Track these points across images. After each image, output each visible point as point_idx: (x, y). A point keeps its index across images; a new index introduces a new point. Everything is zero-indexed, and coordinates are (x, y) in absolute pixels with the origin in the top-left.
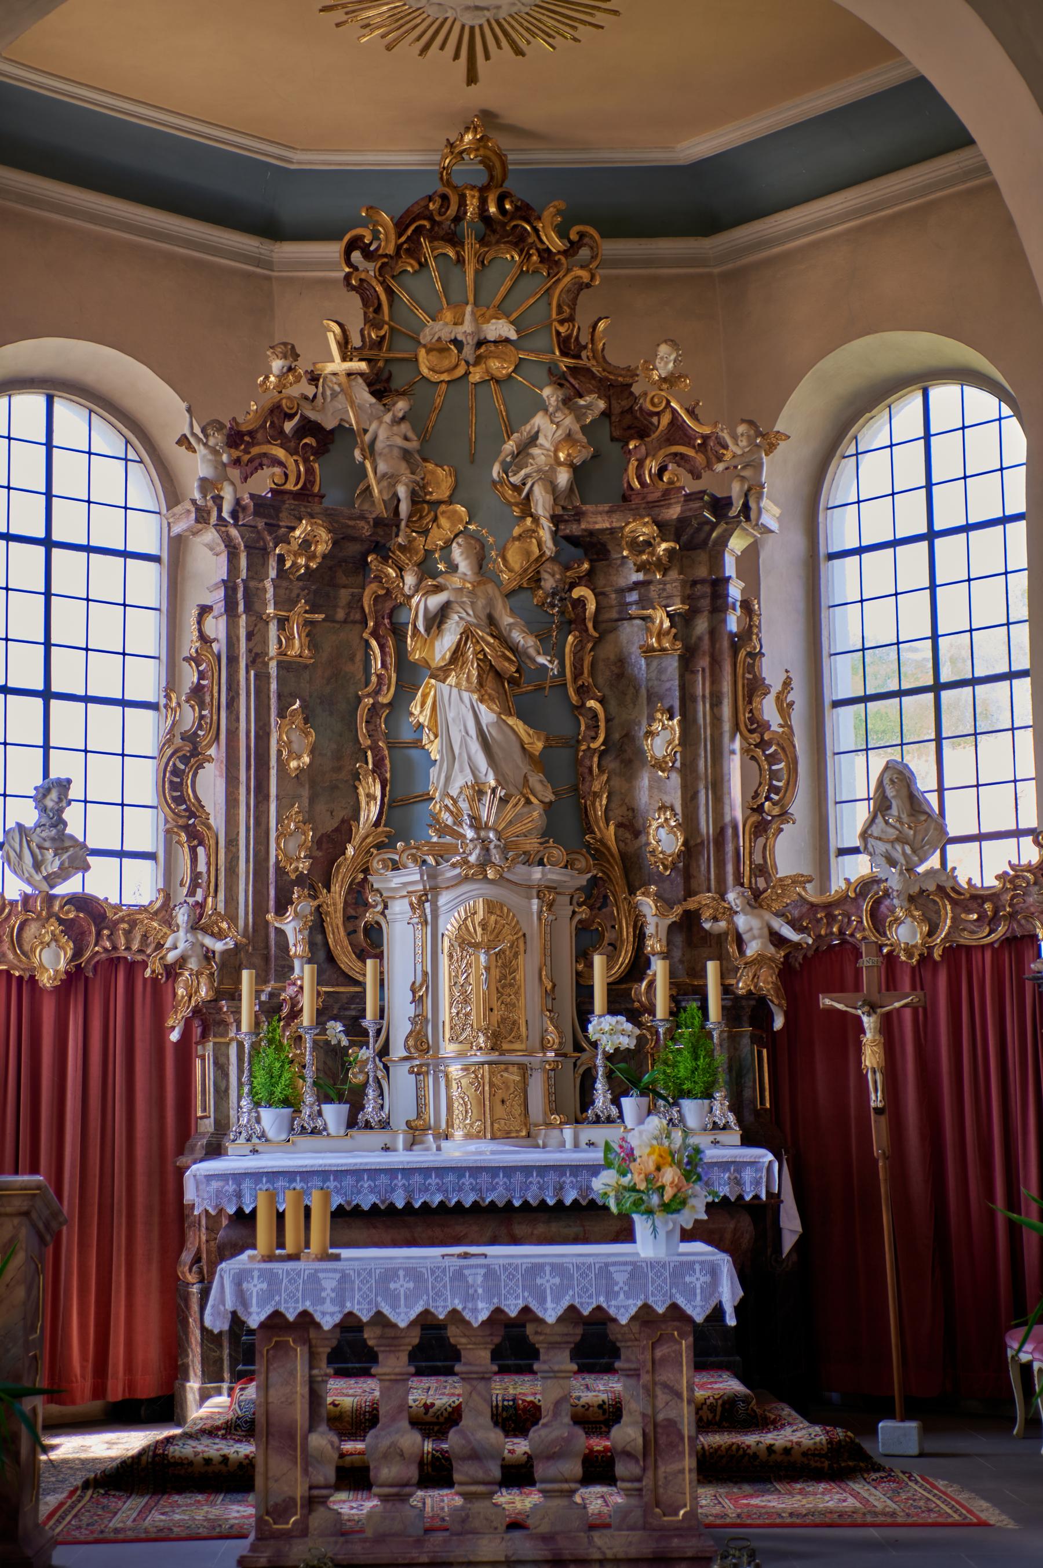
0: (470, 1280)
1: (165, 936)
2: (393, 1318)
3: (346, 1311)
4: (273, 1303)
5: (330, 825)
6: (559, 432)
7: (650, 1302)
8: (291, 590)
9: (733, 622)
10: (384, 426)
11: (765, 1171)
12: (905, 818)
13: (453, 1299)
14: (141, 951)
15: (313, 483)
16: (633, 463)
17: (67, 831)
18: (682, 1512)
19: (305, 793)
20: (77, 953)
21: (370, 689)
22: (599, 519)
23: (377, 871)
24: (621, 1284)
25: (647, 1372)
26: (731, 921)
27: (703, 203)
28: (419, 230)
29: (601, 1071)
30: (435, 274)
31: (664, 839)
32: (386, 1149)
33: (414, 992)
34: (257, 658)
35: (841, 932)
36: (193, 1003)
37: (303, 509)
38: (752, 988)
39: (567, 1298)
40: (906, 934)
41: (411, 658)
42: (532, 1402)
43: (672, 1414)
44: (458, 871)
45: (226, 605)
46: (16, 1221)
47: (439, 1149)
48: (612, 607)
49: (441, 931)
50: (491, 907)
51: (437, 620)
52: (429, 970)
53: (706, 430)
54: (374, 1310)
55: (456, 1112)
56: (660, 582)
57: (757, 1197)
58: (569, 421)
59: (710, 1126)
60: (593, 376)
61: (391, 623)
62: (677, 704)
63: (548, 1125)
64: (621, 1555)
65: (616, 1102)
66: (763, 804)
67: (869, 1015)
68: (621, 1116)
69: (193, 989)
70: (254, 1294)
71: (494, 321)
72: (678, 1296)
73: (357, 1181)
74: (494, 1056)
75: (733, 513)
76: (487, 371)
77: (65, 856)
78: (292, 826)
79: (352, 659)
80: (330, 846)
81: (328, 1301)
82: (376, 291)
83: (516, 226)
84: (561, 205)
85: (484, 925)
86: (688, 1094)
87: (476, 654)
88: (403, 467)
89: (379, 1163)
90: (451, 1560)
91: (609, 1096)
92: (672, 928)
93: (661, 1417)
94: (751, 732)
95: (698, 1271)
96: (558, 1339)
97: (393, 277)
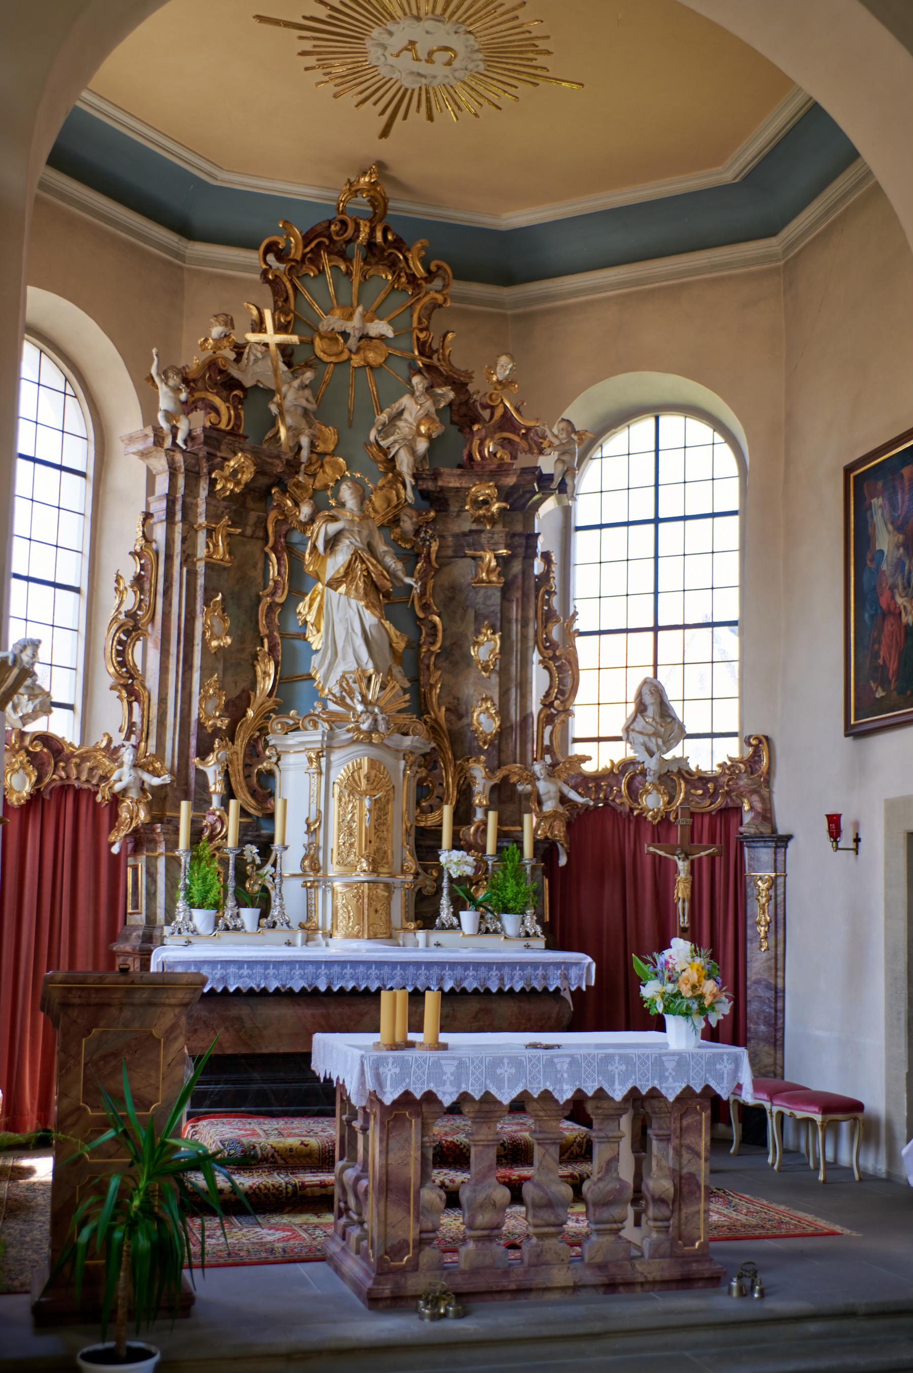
0: (558, 1066)
1: (111, 771)
2: (498, 1097)
3: (462, 1091)
4: (404, 1084)
5: (236, 692)
6: (422, 412)
7: (691, 1085)
8: (218, 508)
9: (538, 566)
10: (292, 390)
11: (585, 972)
12: (658, 719)
13: (545, 1082)
14: (87, 781)
15: (239, 427)
16: (476, 442)
17: (37, 683)
18: (697, 1244)
19: (220, 666)
20: (39, 780)
21: (268, 590)
22: (452, 480)
23: (274, 732)
24: (670, 1071)
25: (677, 1137)
26: (534, 786)
27: (506, 261)
28: (319, 245)
29: (445, 892)
30: (330, 280)
31: (484, 721)
32: (289, 944)
33: (309, 826)
34: (188, 558)
35: (606, 798)
36: (134, 825)
37: (237, 445)
38: (549, 834)
39: (631, 1081)
40: (652, 802)
41: (306, 570)
42: (451, 1142)
43: (693, 1169)
44: (350, 735)
45: (167, 514)
46: (177, 1010)
47: (327, 945)
48: (448, 547)
49: (332, 780)
50: (373, 763)
51: (332, 543)
52: (322, 809)
53: (530, 424)
54: (484, 1091)
55: (340, 918)
56: (489, 532)
57: (579, 989)
58: (429, 404)
59: (523, 934)
60: (441, 374)
61: (286, 542)
62: (498, 624)
63: (405, 929)
64: (658, 1278)
65: (456, 914)
66: (553, 702)
67: (684, 860)
68: (460, 925)
69: (135, 813)
70: (389, 1077)
71: (376, 321)
72: (710, 1079)
73: (291, 970)
74: (372, 877)
75: (554, 485)
76: (365, 360)
77: (37, 701)
78: (211, 691)
79: (255, 567)
80: (236, 708)
81: (448, 1083)
82: (285, 286)
83: (391, 254)
84: (425, 242)
85: (368, 777)
86: (507, 910)
87: (362, 571)
88: (303, 424)
89: (308, 956)
90: (533, 1286)
91: (535, 918)
92: (494, 788)
93: (685, 1171)
94: (546, 648)
95: (725, 1060)
96: (612, 1112)
97: (298, 277)
